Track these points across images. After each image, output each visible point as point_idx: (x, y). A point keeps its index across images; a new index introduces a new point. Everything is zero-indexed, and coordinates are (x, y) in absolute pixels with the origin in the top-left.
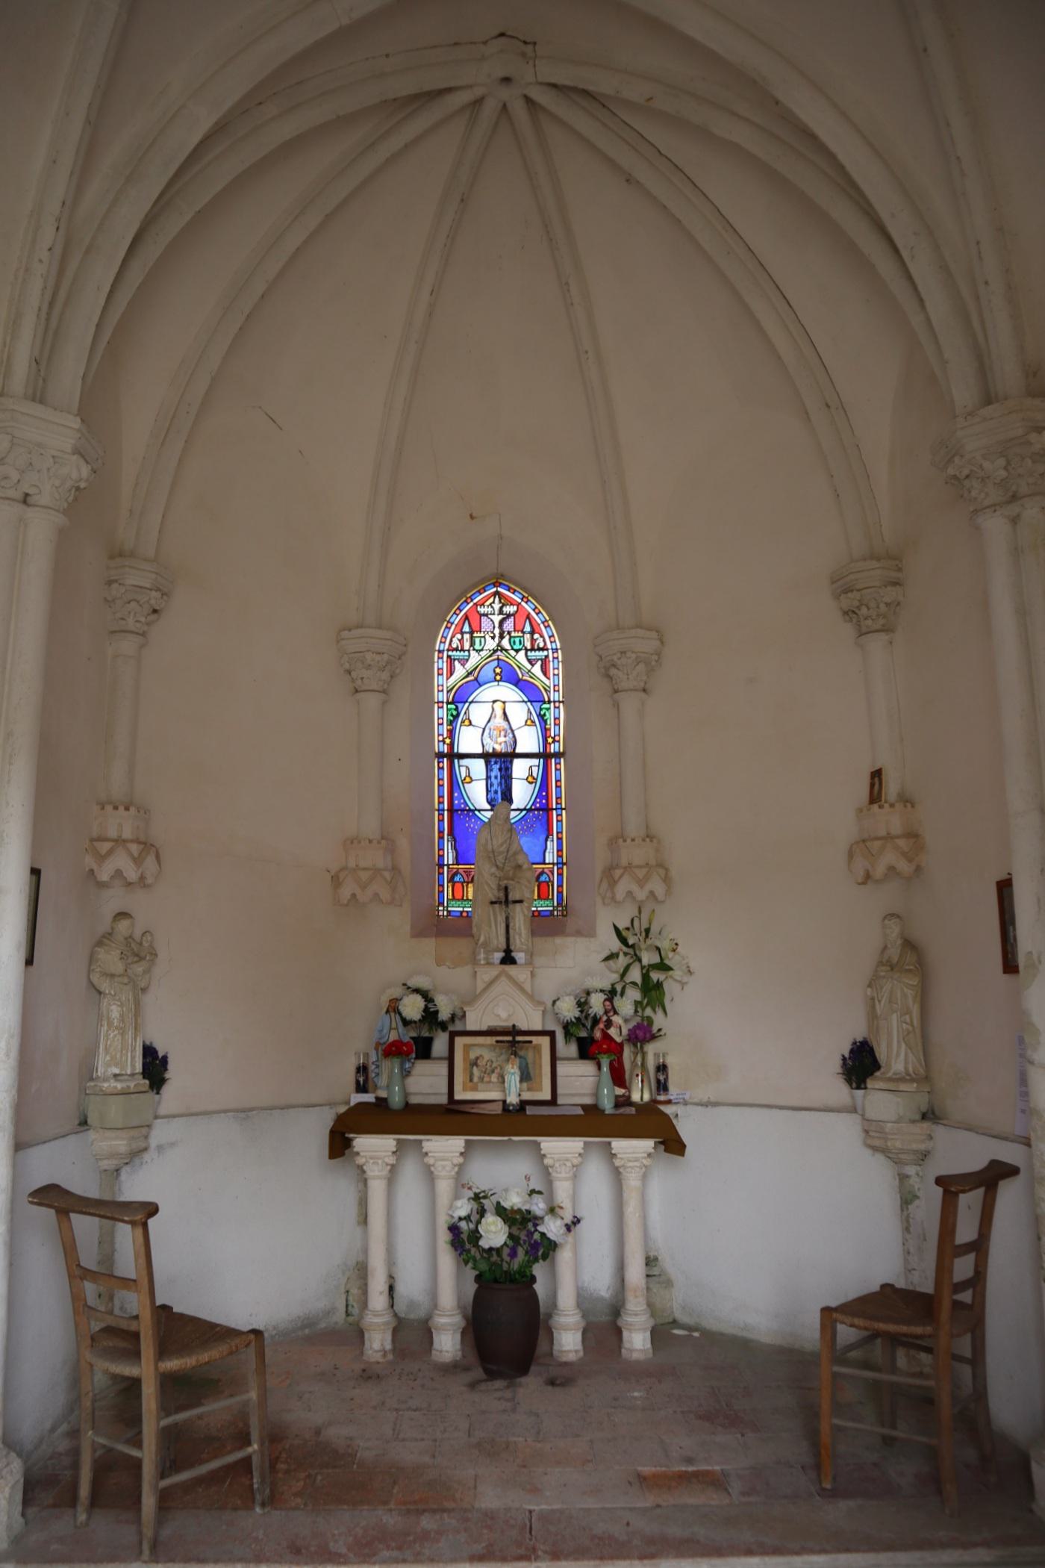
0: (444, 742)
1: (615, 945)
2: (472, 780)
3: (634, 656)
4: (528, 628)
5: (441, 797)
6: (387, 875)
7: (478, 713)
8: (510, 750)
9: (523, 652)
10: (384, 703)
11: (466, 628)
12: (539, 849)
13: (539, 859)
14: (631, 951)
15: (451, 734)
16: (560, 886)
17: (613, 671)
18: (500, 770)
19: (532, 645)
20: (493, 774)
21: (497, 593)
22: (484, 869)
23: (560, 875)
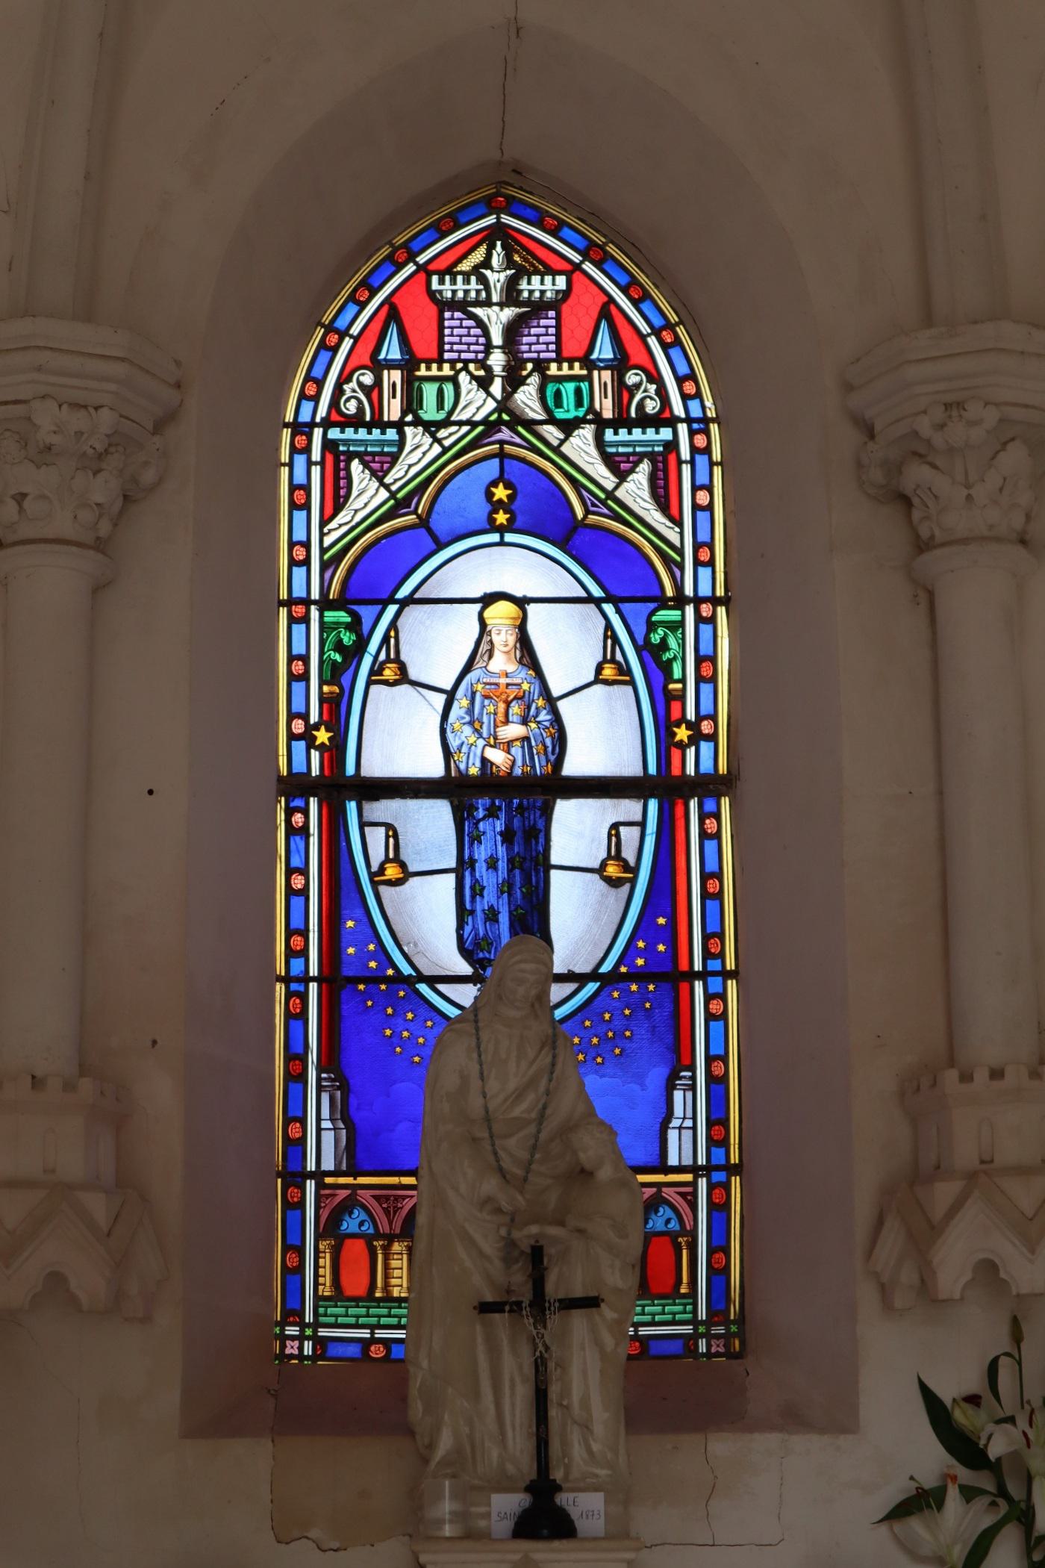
0: (308, 737)
1: (927, 1458)
2: (407, 875)
3: (991, 416)
4: (604, 350)
5: (296, 931)
6: (98, 1206)
7: (437, 643)
8: (541, 767)
9: (587, 432)
10: (99, 589)
11: (392, 350)
12: (645, 1117)
13: (653, 1159)
14: (984, 1481)
15: (336, 711)
16: (719, 1247)
17: (917, 475)
18: (507, 836)
19: (620, 406)
20: (482, 853)
22: (456, 1190)
23: (719, 1209)
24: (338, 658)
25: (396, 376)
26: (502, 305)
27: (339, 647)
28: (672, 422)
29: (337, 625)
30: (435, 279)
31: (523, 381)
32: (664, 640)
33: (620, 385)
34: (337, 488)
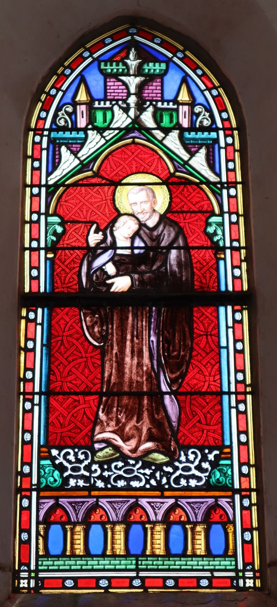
9: (175, 134)
11: (82, 96)
19: (192, 122)
21: (133, 44)
24: (54, 239)
25: (84, 108)
26: (135, 76)
27: (55, 233)
28: (217, 130)
29: (53, 224)
30: (103, 64)
31: (145, 110)
32: (215, 231)
33: (192, 113)
34: (54, 159)
